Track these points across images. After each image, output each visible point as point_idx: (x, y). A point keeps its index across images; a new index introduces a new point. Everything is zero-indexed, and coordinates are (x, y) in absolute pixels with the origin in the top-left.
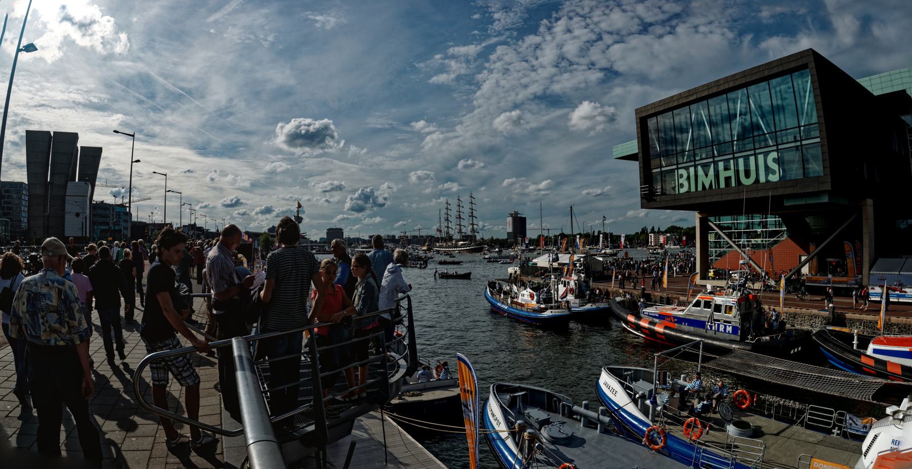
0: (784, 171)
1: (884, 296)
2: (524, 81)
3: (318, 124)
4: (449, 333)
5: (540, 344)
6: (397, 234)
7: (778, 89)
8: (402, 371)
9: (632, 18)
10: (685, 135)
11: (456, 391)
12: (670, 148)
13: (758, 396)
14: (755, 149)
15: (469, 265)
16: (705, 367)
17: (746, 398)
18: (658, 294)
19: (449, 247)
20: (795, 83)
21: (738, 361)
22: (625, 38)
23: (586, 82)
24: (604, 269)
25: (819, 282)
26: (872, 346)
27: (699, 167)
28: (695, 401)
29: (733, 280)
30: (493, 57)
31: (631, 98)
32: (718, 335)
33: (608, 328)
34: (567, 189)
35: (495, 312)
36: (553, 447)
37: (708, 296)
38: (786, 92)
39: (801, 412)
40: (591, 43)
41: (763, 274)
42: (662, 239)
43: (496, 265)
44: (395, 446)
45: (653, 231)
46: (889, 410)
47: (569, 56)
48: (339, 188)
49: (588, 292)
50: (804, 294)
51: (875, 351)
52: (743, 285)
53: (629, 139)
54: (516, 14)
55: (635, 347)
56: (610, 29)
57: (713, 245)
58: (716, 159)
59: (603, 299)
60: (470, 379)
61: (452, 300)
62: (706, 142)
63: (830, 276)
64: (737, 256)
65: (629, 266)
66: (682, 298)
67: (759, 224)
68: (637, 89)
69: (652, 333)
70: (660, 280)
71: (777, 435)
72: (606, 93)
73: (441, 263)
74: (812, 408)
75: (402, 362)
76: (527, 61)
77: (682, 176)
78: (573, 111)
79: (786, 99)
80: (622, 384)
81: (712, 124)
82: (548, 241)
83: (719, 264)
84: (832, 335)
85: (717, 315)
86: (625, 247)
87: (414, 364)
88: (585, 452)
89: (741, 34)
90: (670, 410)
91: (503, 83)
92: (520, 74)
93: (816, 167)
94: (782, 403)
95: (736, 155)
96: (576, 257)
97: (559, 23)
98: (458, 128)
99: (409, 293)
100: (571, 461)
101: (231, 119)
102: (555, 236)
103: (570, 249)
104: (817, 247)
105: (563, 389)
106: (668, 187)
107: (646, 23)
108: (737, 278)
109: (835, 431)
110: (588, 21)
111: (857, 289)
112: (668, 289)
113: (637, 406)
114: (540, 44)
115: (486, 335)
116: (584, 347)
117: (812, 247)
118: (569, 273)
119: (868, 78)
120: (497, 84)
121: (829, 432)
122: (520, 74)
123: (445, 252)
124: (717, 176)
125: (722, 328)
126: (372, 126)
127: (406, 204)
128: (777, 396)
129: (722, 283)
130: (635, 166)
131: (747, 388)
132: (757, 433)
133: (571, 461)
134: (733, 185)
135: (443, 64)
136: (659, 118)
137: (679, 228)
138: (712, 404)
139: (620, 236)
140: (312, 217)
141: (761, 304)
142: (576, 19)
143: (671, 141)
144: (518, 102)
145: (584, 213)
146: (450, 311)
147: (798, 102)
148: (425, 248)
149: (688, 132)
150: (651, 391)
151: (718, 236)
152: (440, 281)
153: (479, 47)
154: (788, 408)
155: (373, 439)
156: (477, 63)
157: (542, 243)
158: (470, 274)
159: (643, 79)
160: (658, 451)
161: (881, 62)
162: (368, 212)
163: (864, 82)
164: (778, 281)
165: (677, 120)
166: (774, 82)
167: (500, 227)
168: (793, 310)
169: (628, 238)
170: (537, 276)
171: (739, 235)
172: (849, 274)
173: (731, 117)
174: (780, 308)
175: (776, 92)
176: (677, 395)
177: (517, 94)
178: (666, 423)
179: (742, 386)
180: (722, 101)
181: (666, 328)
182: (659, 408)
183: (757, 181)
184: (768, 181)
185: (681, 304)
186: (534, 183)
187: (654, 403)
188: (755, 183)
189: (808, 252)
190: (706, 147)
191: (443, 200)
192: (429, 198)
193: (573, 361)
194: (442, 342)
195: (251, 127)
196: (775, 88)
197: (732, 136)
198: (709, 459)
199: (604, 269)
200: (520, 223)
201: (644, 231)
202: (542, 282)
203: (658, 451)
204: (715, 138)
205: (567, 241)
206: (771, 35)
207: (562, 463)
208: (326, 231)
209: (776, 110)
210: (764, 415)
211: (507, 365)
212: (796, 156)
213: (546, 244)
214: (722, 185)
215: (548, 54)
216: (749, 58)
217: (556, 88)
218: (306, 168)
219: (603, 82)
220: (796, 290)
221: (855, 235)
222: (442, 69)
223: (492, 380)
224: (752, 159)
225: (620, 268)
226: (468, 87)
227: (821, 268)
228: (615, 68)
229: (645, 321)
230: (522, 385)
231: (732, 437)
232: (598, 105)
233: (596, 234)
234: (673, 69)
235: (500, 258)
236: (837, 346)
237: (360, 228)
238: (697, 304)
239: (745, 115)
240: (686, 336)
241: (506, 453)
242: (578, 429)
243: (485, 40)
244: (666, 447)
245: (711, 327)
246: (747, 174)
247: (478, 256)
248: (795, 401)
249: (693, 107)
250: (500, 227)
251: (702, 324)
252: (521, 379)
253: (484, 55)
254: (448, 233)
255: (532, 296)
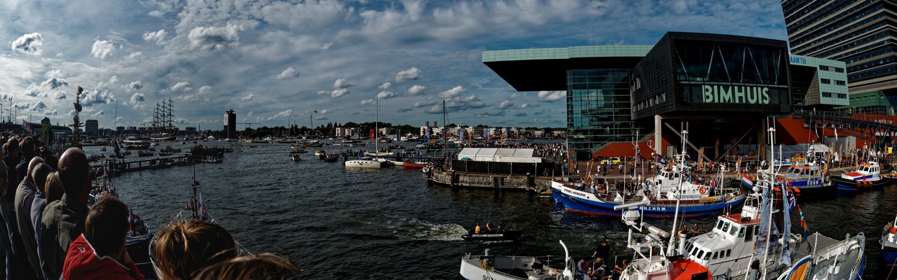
2: (210, 20)
77: (707, 90)
89: (347, 7)
200: (232, 117)
201: (330, 125)
214: (737, 101)
219: (258, 28)
224: (755, 88)
228: (266, 19)
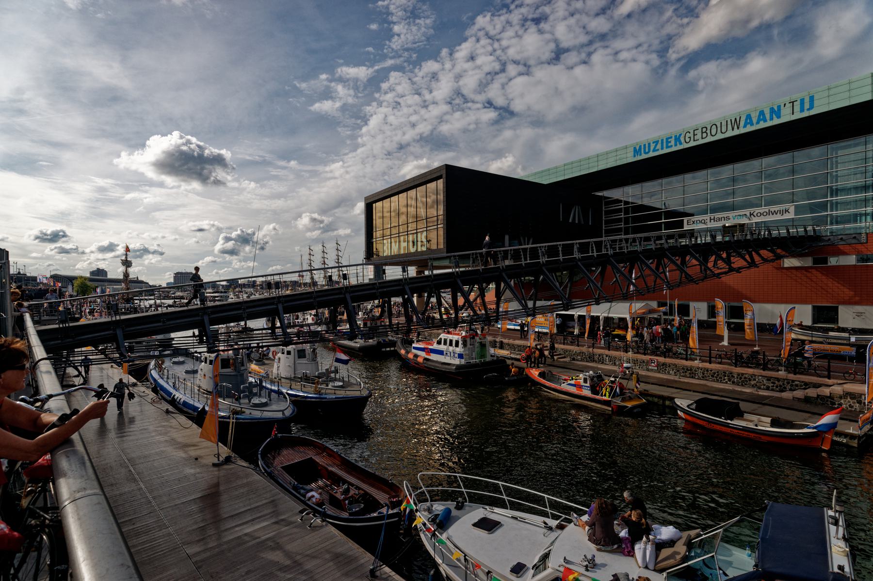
2: (414, 118)
30: (384, 86)
47: (465, 91)
54: (419, 29)
56: (517, 57)
76: (419, 94)
91: (391, 119)
101: (22, 120)
110: (496, 45)
120: (385, 121)
122: (411, 110)
153: (371, 70)
156: (366, 92)
177: (404, 134)
195: (61, 136)
208: (173, 275)
215: (443, 89)
217: (445, 128)
219: (496, 122)
222: (327, 94)
253: (374, 83)
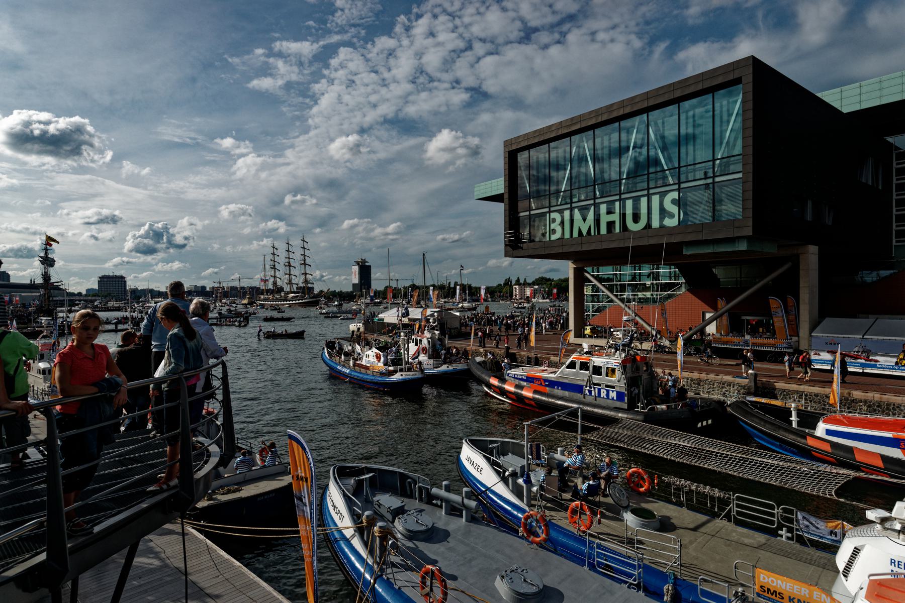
0: (685, 213)
1: (838, 364)
2: (373, 98)
3: (63, 123)
4: (277, 406)
5: (388, 414)
6: (209, 285)
7: (691, 113)
8: (214, 461)
9: (513, 20)
10: (561, 173)
11: (287, 480)
12: (542, 187)
13: (659, 477)
14: (648, 189)
15: (302, 321)
16: (586, 440)
17: (644, 480)
18: (524, 353)
19: (277, 303)
20: (717, 105)
21: (628, 432)
22: (500, 48)
23: (447, 105)
24: (462, 325)
25: (732, 343)
26: (821, 429)
27: (576, 211)
28: (579, 481)
29: (615, 339)
30: (334, 62)
31: (502, 126)
32: (599, 401)
33: (468, 392)
34: (420, 234)
35: (335, 376)
36: (410, 544)
37: (585, 357)
38: (702, 117)
39: (724, 503)
40: (457, 53)
41: (654, 333)
42: (528, 292)
43: (334, 320)
44: (201, 571)
45: (518, 282)
46: (871, 515)
47: (430, 69)
48: (113, 220)
49: (443, 352)
50: (710, 357)
51: (829, 432)
52: (628, 345)
53: (493, 176)
55: (500, 414)
57: (590, 299)
58: (597, 201)
59: (460, 359)
60: (304, 463)
61: (281, 364)
62: (586, 181)
63: (748, 337)
64: (621, 312)
65: (490, 322)
66: (553, 358)
67: (649, 276)
68: (508, 115)
69: (520, 398)
70: (527, 338)
71: (695, 529)
72: (472, 120)
73: (266, 320)
74: (738, 498)
75: (214, 449)
76: (376, 72)
77: (554, 220)
78: (430, 141)
79: (700, 125)
80: (488, 459)
81: (595, 159)
82: (396, 293)
83: (597, 320)
84: (756, 407)
85: (596, 378)
86: (486, 300)
87: (230, 449)
88: (450, 549)
89: (652, 42)
90: (550, 492)
91: (346, 98)
92: (369, 89)
93: (732, 209)
94: (693, 488)
95: (623, 196)
96: (429, 312)
97: (421, 21)
98: (289, 153)
99: (224, 358)
100: (434, 562)
102: (405, 288)
103: (422, 303)
104: (728, 302)
105: (416, 467)
106: (537, 234)
107: (531, 28)
108: (620, 336)
109: (783, 532)
111: (789, 354)
112: (536, 348)
113: (507, 485)
114: (394, 50)
115: (325, 405)
116: (441, 415)
117: (721, 303)
118: (421, 330)
119: (838, 90)
121: (774, 533)
122: (369, 89)
123: (271, 306)
124: (597, 221)
125: (603, 394)
126: (166, 138)
127: (216, 246)
128: (686, 479)
129: (602, 342)
130: (500, 208)
131: (644, 466)
132: (666, 525)
133: (434, 562)
134: (617, 230)
135: (266, 63)
136: (532, 151)
137: (549, 280)
138: (599, 484)
139: (480, 288)
140: (67, 259)
141: (651, 367)
142: (443, 18)
143: (544, 177)
144: (365, 126)
145: (438, 262)
146: (278, 378)
147: (717, 129)
148: (245, 301)
149: (565, 169)
150: (523, 468)
151: (595, 289)
152: (265, 342)
153: (315, 46)
154: (705, 496)
155: (166, 566)
156: (313, 69)
157: (390, 295)
158: (303, 332)
159: (517, 103)
160: (539, 544)
161: (871, 64)
162: (160, 255)
163: (830, 97)
164: (674, 341)
165: (553, 154)
166: (686, 104)
167: (343, 278)
168: (696, 375)
169: (488, 290)
170: (384, 334)
171: (623, 288)
172: (778, 336)
173: (621, 151)
174: (678, 372)
175: (687, 118)
176: (555, 473)
177: (365, 116)
178: (545, 507)
179: (636, 464)
180: (613, 131)
181: (535, 392)
182: (535, 489)
183: (648, 226)
184: (662, 227)
185: (551, 365)
186: (380, 226)
187: (528, 482)
188: (645, 228)
189: (715, 308)
190: (587, 187)
191: (267, 242)
192: (249, 239)
193: (428, 432)
194: (267, 417)
196: (687, 112)
197: (620, 173)
198: (607, 558)
199: (462, 325)
200: (365, 271)
201: (508, 283)
202: (389, 340)
203: (539, 544)
204: (599, 176)
205: (417, 293)
206: (694, 41)
207: (423, 566)
209: (682, 140)
210: (670, 502)
211: (349, 441)
212: (706, 196)
213: (394, 297)
214: (604, 230)
215: (404, 65)
216: (659, 75)
217: (411, 110)
218: (58, 188)
219: (468, 105)
220: (698, 351)
221: (788, 288)
222: (266, 71)
223: (333, 461)
224: (644, 201)
225: (480, 324)
226: (301, 99)
227: (735, 326)
229: (511, 385)
230: (369, 466)
231: (633, 530)
232: (460, 134)
233: (452, 285)
234: (555, 90)
235: (340, 312)
236: (766, 422)
237: (151, 275)
238: (572, 365)
239: (641, 147)
240: (560, 402)
241: (353, 558)
242: (440, 518)
243: (323, 37)
244: (549, 539)
245: (590, 392)
246: (636, 218)
247: (313, 311)
248: (713, 486)
249: (575, 138)
250: (343, 278)
251: (578, 389)
252: (367, 458)
254: (275, 283)
255: (378, 357)
